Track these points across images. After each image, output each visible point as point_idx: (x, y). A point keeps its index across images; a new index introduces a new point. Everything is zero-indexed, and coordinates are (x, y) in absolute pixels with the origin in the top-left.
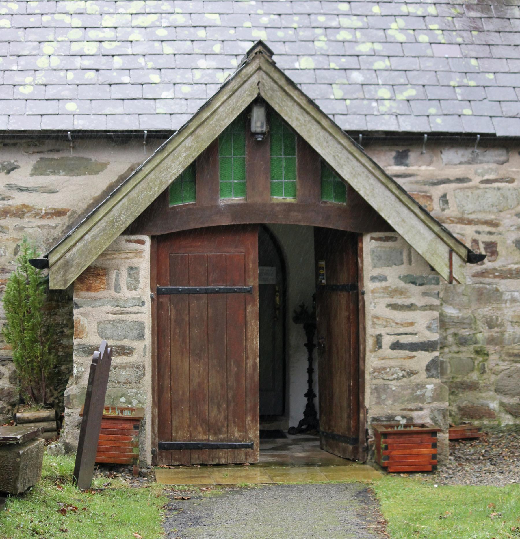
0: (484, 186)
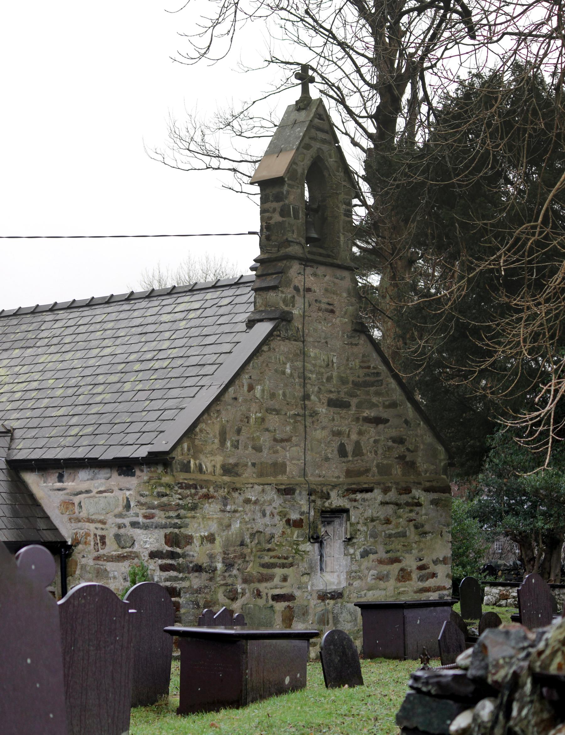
0: (98, 495)
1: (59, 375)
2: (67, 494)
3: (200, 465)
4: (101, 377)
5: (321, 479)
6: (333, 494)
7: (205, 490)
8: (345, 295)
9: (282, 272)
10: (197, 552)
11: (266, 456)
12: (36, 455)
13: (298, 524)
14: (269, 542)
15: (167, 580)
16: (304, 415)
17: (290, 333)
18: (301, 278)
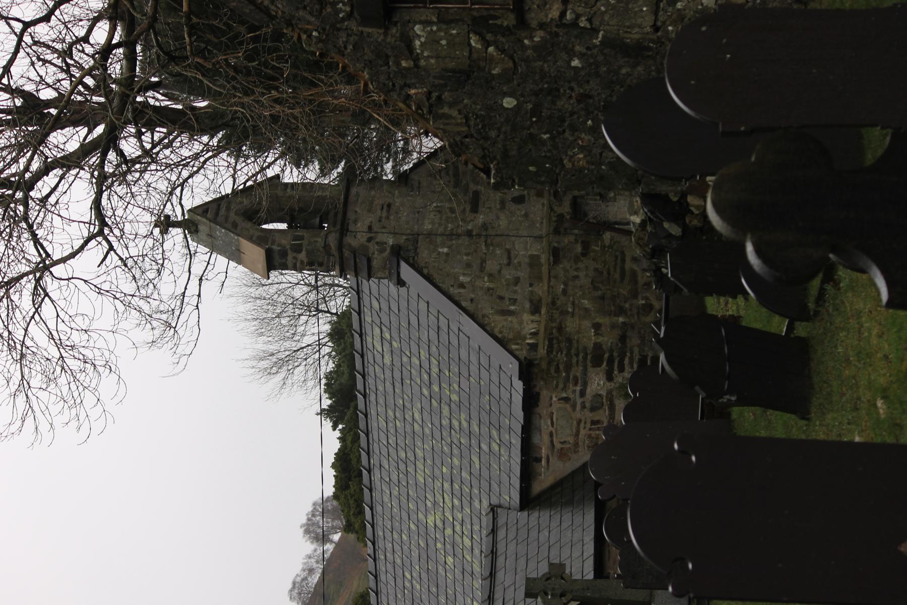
1: (438, 462)
2: (552, 454)
3: (531, 334)
4: (444, 422)
5: (544, 221)
6: (559, 210)
7: (554, 331)
8: (373, 193)
9: (354, 252)
10: (608, 340)
11: (523, 274)
12: (516, 483)
13: (586, 246)
14: (601, 273)
15: (632, 367)
16: (486, 236)
17: (411, 247)
18: (359, 235)
